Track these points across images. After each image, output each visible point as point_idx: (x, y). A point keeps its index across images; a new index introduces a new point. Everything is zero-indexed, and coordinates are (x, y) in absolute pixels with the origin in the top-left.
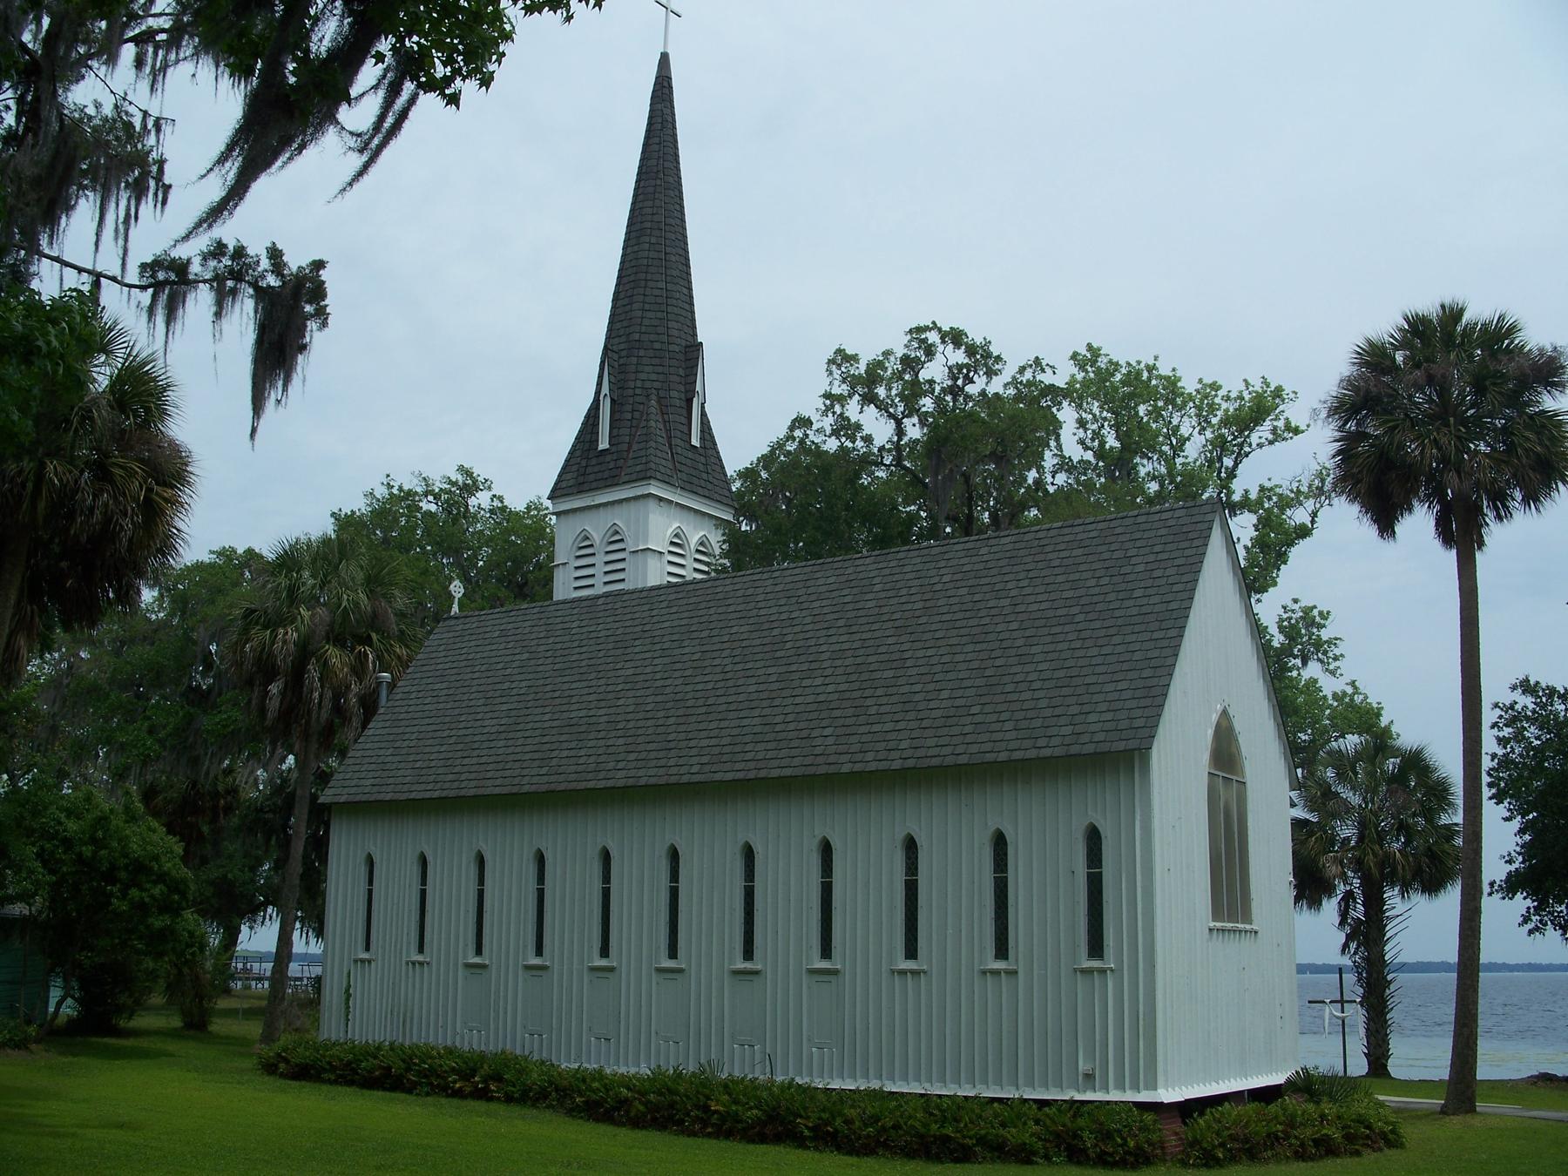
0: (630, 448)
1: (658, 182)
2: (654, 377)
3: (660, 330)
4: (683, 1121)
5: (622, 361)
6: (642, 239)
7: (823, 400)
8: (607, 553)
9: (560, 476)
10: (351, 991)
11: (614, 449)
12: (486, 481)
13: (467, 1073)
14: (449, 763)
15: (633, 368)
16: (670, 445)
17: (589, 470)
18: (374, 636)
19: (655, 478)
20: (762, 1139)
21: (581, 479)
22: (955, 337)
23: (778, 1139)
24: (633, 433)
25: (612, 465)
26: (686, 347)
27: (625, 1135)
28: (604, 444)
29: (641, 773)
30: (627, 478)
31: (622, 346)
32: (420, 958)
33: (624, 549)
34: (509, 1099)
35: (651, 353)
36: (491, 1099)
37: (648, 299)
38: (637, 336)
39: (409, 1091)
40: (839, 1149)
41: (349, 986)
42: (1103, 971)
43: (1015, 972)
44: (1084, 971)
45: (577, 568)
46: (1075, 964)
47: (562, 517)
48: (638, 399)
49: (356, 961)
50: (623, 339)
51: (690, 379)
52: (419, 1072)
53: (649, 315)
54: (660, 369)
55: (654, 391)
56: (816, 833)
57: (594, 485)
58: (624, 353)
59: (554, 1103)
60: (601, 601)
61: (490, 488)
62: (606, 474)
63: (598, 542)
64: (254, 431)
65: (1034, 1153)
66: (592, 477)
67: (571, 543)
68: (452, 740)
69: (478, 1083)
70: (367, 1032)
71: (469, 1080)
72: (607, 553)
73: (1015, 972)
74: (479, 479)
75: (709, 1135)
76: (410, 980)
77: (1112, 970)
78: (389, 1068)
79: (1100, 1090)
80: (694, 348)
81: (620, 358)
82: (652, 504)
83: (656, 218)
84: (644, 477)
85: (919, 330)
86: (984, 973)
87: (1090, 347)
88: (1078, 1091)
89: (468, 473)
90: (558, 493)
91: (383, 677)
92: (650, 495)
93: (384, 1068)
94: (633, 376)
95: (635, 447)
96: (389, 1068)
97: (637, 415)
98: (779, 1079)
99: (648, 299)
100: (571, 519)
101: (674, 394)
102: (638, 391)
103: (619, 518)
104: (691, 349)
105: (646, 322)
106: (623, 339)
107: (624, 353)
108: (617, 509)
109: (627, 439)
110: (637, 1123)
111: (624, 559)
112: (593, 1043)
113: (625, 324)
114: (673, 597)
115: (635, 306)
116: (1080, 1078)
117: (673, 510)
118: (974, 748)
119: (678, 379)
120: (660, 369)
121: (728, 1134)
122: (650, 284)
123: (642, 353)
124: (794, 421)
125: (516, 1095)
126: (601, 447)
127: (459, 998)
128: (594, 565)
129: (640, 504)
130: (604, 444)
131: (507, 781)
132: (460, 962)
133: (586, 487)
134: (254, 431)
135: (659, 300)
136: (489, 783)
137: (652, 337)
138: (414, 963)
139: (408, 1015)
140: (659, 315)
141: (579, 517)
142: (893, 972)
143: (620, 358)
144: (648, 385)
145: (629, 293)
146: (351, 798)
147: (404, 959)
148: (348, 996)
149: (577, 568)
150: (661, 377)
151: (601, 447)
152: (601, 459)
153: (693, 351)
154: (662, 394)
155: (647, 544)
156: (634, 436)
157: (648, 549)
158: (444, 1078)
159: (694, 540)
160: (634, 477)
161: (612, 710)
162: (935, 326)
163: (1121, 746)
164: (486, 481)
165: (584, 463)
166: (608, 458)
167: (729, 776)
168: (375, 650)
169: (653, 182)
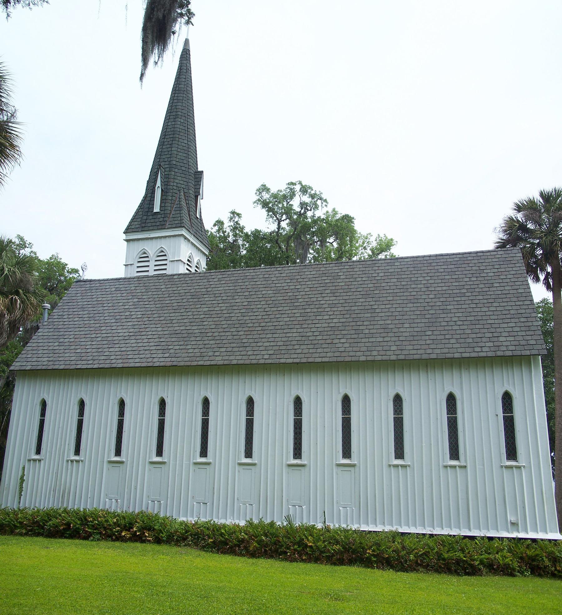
0: (171, 213)
1: (185, 96)
2: (182, 182)
3: (185, 162)
4: (286, 553)
5: (166, 173)
6: (176, 120)
7: (230, 214)
8: (156, 261)
9: (130, 223)
10: (25, 478)
11: (162, 212)
12: (30, 243)
13: (128, 527)
14: (100, 350)
15: (172, 177)
16: (189, 215)
17: (148, 221)
18: (21, 291)
19: (185, 228)
20: (341, 562)
21: (143, 225)
22: (304, 190)
23: (351, 562)
24: (172, 206)
25: (161, 219)
26: (195, 172)
27: (326, 568)
28: (157, 209)
29: (231, 358)
30: (170, 226)
31: (166, 166)
32: (77, 458)
33: (167, 260)
34: (158, 541)
35: (181, 171)
36: (143, 541)
37: (179, 147)
38: (174, 162)
39: (86, 538)
40: (392, 567)
41: (23, 475)
42: (519, 467)
43: (465, 467)
44: (507, 467)
45: (138, 267)
46: (444, 463)
47: (131, 242)
48: (175, 191)
49: (29, 460)
50: (167, 163)
51: (198, 187)
52: (93, 526)
53: (180, 154)
54: (185, 179)
55: (182, 189)
56: (341, 391)
57: (151, 228)
58: (167, 169)
59: (190, 543)
60: (175, 277)
61: (31, 248)
62: (158, 224)
63: (151, 255)
64: (142, 75)
65: (514, 569)
66: (149, 225)
67: (135, 256)
68: (99, 339)
69: (136, 532)
70: (36, 501)
71: (129, 531)
72: (156, 261)
73: (465, 467)
74: (27, 242)
75: (303, 561)
76: (69, 471)
77: (524, 467)
78: (68, 524)
79: (522, 531)
80: (199, 173)
81: (165, 171)
82: (182, 239)
83: (183, 111)
84: (180, 226)
85: (292, 184)
86: (446, 467)
87: (334, 210)
88: (509, 532)
89: (22, 239)
90: (129, 231)
91: (47, 306)
92: (182, 235)
93: (65, 524)
94: (172, 180)
95: (173, 212)
96: (68, 524)
97: (174, 198)
98: (203, 520)
99: (179, 147)
100: (136, 244)
101: (191, 192)
102: (175, 188)
103: (164, 244)
104: (198, 173)
105: (178, 157)
106: (167, 163)
107: (167, 169)
108: (163, 240)
109: (169, 208)
110: (253, 555)
111: (166, 264)
112: (241, 507)
113: (168, 156)
114: (221, 276)
115: (173, 149)
116: (509, 525)
117: (190, 245)
118: (438, 351)
119: (192, 185)
120: (185, 179)
121: (317, 560)
122: (180, 140)
123: (176, 170)
124: (217, 221)
125: (164, 539)
126: (155, 211)
127: (103, 482)
128: (149, 266)
129: (177, 239)
130: (157, 209)
131: (144, 360)
132: (106, 460)
133: (146, 229)
134: (142, 75)
135: (185, 148)
136: (130, 361)
137: (182, 164)
138: (72, 461)
139: (67, 491)
140: (184, 155)
141: (141, 243)
142: (390, 466)
143: (165, 171)
144: (179, 185)
145: (170, 142)
146: (34, 368)
147: (65, 459)
148: (22, 480)
149: (138, 267)
150: (185, 183)
151: (155, 211)
152: (155, 217)
153: (199, 176)
154: (186, 191)
155: (180, 258)
156: (173, 207)
157: (180, 260)
158: (111, 530)
159: (196, 260)
160: (174, 226)
161: (201, 327)
162: (300, 183)
163: (528, 353)
164: (30, 243)
165: (145, 217)
166: (159, 216)
167: (290, 361)
168: (21, 298)
169: (182, 95)
